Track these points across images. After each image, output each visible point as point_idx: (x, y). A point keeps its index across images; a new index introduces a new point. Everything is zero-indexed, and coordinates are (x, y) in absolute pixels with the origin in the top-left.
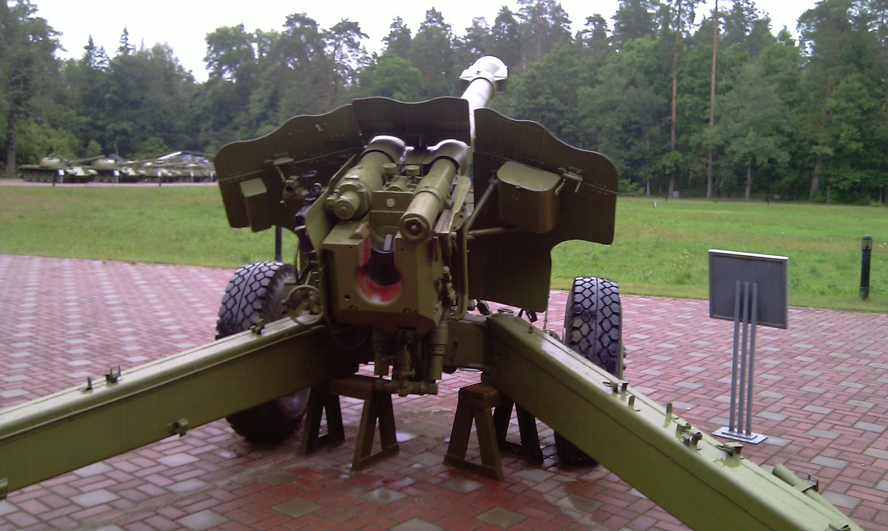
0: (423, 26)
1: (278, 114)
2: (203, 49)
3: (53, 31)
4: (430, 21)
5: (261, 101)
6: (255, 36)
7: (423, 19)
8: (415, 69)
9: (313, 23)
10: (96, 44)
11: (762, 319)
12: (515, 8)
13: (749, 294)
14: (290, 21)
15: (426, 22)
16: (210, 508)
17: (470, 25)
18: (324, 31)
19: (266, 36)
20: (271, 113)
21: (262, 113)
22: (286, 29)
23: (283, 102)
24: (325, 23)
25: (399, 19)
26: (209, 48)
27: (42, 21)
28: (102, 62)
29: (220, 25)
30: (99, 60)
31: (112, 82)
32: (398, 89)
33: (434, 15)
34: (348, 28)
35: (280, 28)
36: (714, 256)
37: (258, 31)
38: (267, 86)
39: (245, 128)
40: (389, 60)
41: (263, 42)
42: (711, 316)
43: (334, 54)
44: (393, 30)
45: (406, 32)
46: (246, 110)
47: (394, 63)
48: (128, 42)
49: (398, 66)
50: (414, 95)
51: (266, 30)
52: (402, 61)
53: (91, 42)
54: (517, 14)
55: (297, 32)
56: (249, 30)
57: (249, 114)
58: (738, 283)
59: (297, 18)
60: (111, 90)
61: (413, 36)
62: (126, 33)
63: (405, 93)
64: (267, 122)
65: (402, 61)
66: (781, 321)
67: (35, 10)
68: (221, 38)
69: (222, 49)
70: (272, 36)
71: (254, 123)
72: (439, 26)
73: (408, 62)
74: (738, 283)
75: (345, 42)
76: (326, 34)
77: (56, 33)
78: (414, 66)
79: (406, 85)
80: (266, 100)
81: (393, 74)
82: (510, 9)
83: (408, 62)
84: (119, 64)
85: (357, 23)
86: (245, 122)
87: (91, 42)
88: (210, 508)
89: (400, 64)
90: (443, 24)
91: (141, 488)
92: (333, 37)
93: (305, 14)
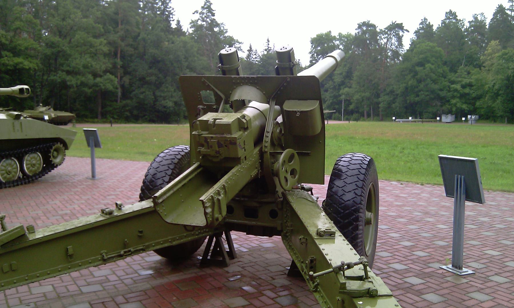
0: (443, 22)
1: (352, 81)
2: (308, 47)
3: (238, 42)
4: (449, 18)
5: (341, 74)
6: (338, 37)
7: (443, 17)
8: (440, 49)
9: (374, 26)
10: (254, 49)
11: (469, 198)
12: (507, 5)
13: (462, 181)
14: (360, 27)
15: (445, 19)
16: (140, 301)
17: (472, 19)
18: (381, 30)
19: (344, 37)
20: (347, 81)
21: (343, 81)
22: (357, 31)
23: (356, 74)
24: (381, 25)
25: (425, 19)
26: (312, 46)
27: (425, 31)
28: (256, 58)
29: (319, 33)
30: (254, 57)
31: (261, 68)
32: (429, 62)
33: (451, 14)
34: (396, 28)
35: (353, 31)
36: (441, 158)
37: (340, 34)
38: (345, 65)
39: (331, 90)
40: (423, 44)
41: (342, 40)
42: (447, 196)
43: (386, 44)
44: (421, 26)
45: (430, 26)
46: (332, 80)
47: (426, 46)
48: (269, 46)
49: (428, 48)
50: (439, 65)
51: (344, 33)
52: (431, 44)
53: (251, 48)
54: (508, 9)
55: (364, 32)
56: (335, 33)
57: (334, 82)
58: (456, 175)
59: (364, 24)
60: (260, 73)
61: (435, 28)
62: (268, 41)
63: (433, 64)
64: (344, 86)
65: (431, 44)
66: (478, 198)
67: (226, 32)
68: (319, 40)
69: (318, 46)
70: (348, 36)
71: (337, 87)
72: (454, 21)
73: (435, 44)
74: (456, 175)
75: (393, 35)
76: (382, 32)
77: (240, 43)
78: (439, 47)
79: (434, 59)
80: (344, 74)
81: (426, 52)
82: (504, 6)
83: (435, 44)
84: (265, 58)
85: (402, 24)
86: (332, 87)
87: (251, 48)
88: (140, 301)
89: (430, 46)
90: (457, 20)
91: (425, 282)
92: (386, 33)
93: (369, 21)
